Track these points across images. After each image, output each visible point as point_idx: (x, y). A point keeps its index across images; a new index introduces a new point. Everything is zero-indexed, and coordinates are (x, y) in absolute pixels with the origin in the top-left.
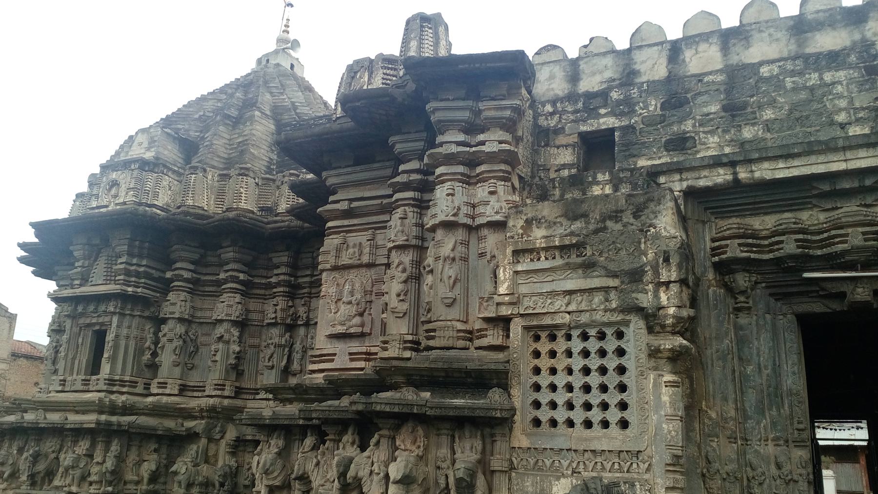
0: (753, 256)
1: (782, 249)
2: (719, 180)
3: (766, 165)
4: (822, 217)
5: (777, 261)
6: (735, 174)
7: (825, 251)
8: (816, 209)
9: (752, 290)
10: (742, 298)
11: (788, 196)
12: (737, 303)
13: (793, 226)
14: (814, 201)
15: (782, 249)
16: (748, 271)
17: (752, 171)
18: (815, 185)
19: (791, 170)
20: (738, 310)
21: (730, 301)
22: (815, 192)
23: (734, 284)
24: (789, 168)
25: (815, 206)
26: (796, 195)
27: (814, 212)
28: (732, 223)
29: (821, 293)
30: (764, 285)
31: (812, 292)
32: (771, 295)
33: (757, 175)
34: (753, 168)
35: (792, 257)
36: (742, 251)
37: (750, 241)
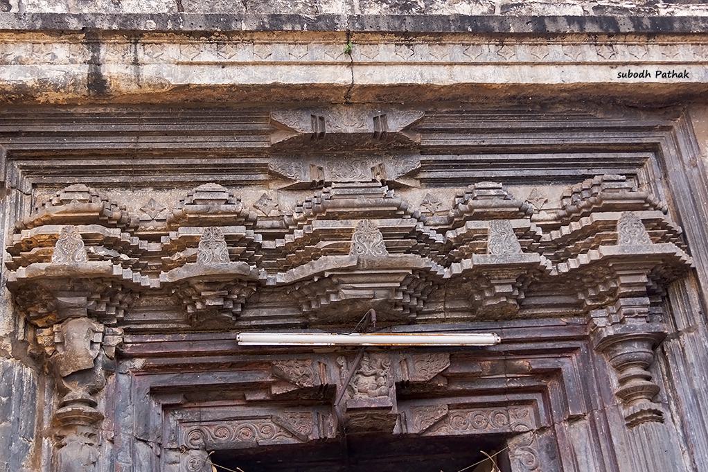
0: (117, 270)
1: (193, 259)
2: (55, 74)
3: (172, 51)
4: (289, 203)
5: (179, 293)
6: (95, 63)
7: (297, 273)
8: (274, 186)
9: (108, 373)
10: (78, 391)
11: (213, 143)
12: (64, 405)
13: (223, 207)
14: (274, 164)
15: (193, 259)
16: (100, 318)
17: (136, 63)
18: (279, 118)
19: (228, 70)
20: (64, 423)
21: (48, 403)
22: (276, 139)
23: (61, 351)
24: (223, 65)
25: (275, 176)
26: (233, 144)
27: (272, 191)
28: (78, 196)
29: (276, 390)
30: (139, 363)
31: (256, 387)
32: (155, 392)
33: (148, 72)
34: (141, 55)
35: (214, 282)
36: (92, 257)
37: (115, 233)
